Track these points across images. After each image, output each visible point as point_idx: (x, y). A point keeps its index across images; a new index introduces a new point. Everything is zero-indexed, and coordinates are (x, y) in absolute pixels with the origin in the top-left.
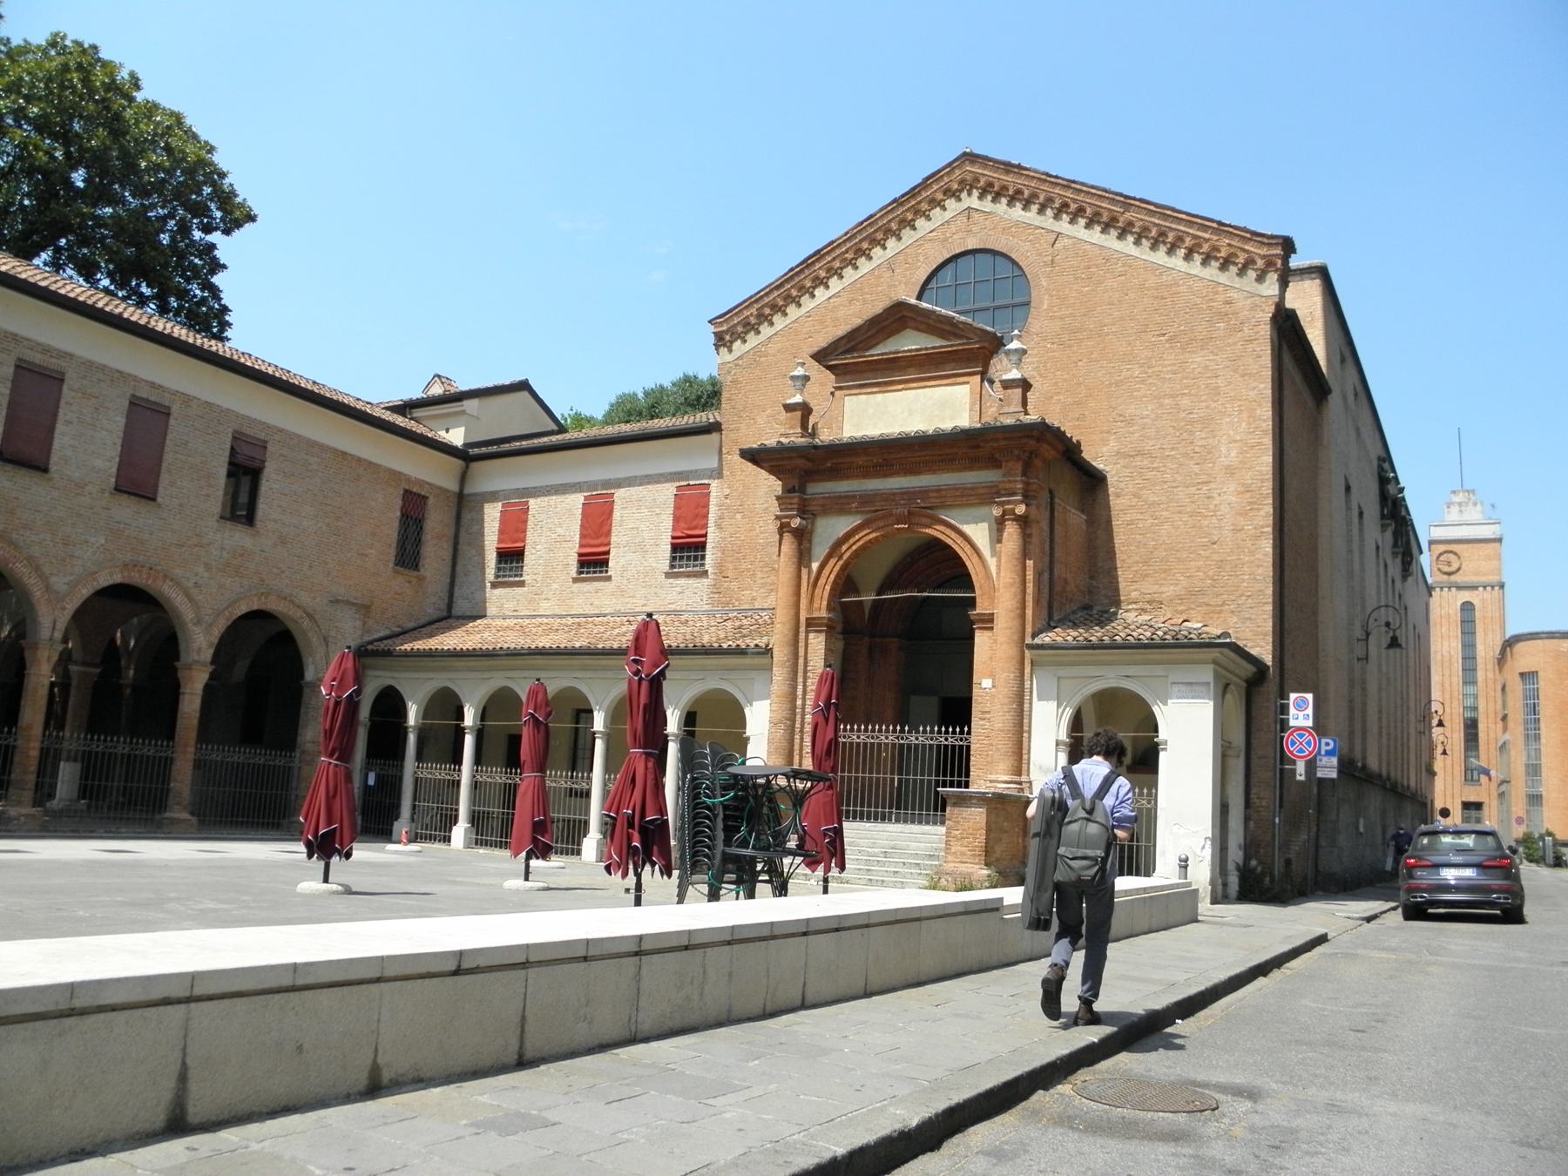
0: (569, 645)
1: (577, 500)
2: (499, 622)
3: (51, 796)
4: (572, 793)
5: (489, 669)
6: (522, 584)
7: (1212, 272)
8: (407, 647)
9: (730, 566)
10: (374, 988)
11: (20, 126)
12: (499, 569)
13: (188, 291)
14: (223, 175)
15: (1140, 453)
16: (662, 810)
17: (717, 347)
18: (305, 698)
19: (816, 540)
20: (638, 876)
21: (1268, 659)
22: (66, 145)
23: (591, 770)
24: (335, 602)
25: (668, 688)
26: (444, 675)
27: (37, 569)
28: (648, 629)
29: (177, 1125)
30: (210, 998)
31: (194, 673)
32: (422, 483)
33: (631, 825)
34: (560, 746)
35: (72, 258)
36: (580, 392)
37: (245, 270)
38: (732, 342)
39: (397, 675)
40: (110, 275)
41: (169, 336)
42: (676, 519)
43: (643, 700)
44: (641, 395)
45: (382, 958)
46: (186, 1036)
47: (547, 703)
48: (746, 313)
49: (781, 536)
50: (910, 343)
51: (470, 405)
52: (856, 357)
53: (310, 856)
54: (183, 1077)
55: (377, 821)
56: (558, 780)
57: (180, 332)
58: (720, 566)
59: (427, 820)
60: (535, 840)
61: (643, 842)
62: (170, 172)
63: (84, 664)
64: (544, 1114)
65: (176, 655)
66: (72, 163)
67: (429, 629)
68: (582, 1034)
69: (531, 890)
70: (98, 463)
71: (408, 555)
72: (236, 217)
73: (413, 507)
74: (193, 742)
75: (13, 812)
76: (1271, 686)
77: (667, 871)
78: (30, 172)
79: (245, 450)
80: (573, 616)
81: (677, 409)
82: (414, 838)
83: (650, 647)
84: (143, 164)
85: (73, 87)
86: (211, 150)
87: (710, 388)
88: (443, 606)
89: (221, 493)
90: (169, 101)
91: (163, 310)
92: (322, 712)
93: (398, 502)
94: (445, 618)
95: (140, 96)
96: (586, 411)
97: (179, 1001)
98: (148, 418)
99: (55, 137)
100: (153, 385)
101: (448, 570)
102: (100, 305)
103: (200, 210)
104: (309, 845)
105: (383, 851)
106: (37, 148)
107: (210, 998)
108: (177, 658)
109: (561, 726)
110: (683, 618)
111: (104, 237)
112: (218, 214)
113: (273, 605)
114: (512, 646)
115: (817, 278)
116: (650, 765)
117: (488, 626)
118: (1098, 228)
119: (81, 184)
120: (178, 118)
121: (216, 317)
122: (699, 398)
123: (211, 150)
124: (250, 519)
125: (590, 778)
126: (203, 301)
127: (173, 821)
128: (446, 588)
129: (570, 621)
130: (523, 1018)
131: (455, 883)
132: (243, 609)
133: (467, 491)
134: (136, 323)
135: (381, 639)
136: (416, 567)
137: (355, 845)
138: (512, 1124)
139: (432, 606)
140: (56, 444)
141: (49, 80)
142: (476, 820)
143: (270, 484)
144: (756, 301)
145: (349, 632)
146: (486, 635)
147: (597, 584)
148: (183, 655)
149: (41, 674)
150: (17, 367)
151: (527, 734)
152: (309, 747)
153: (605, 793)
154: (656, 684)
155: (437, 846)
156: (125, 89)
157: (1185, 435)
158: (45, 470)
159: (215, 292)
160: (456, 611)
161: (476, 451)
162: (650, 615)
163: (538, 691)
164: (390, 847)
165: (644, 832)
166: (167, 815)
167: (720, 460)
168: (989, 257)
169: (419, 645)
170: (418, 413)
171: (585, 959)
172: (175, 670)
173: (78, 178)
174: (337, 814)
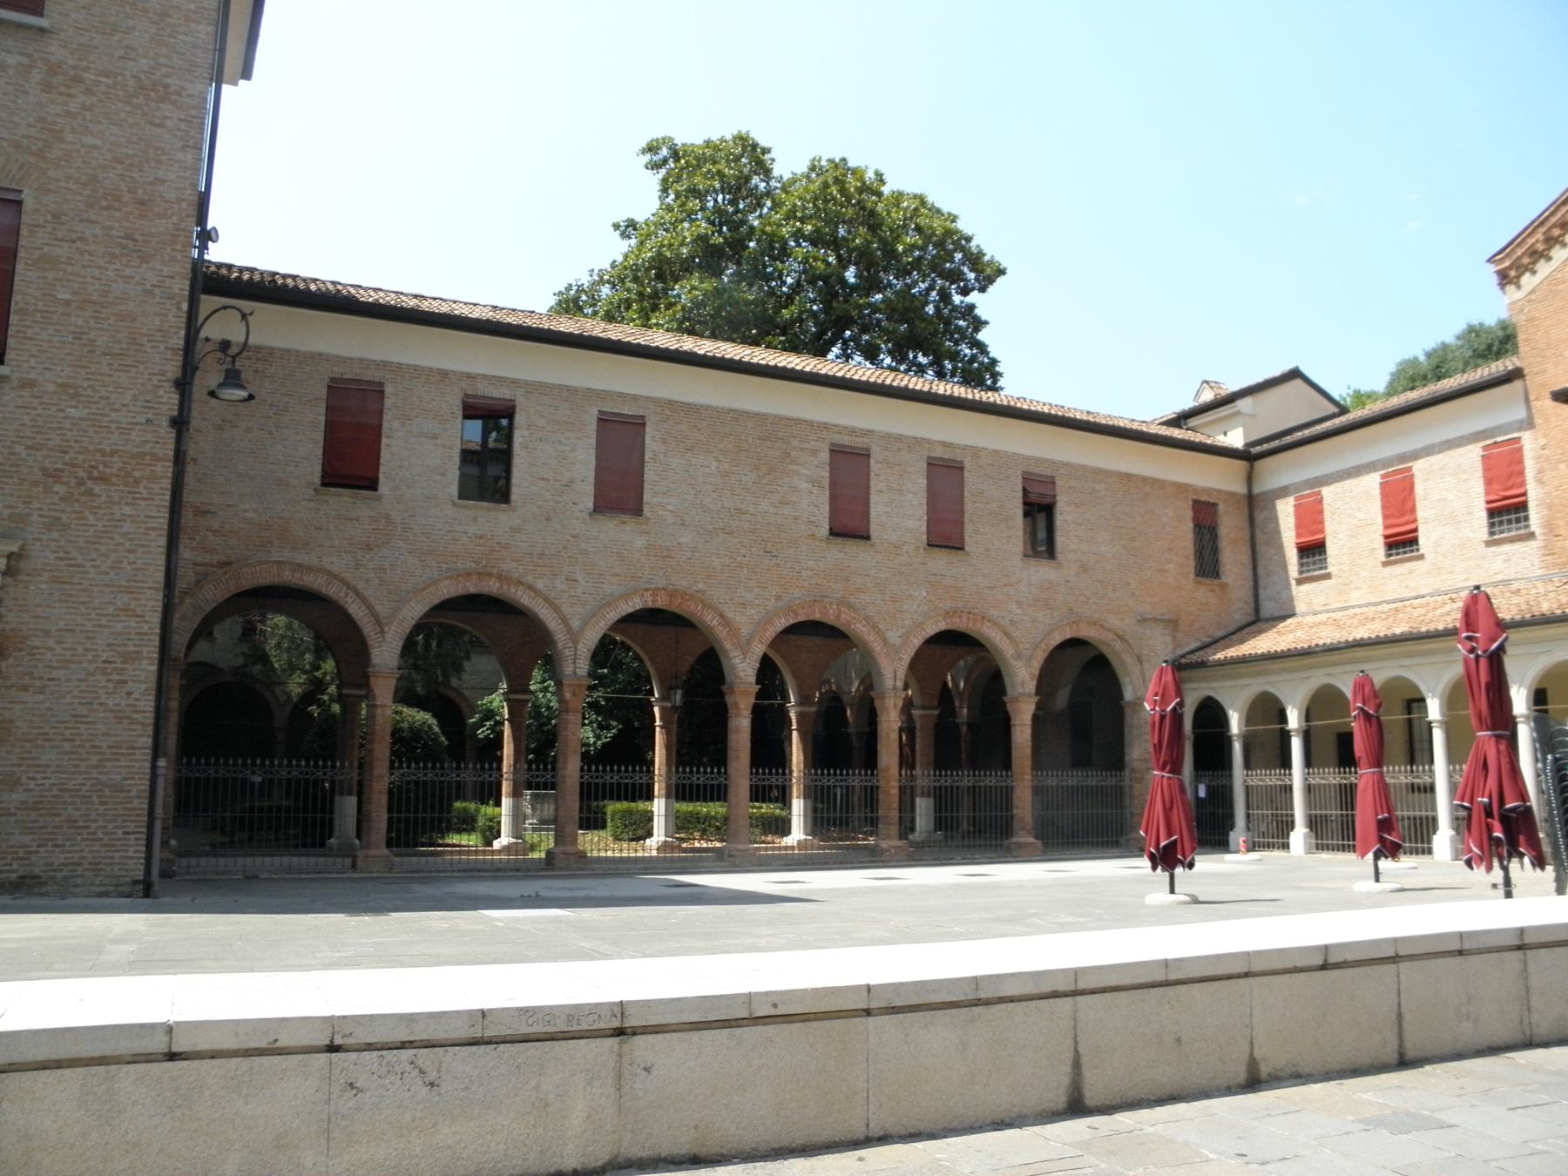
0: (1389, 633)
1: (1373, 481)
2: (1310, 619)
3: (912, 830)
4: (1413, 788)
5: (1309, 667)
6: (1328, 576)
8: (1220, 656)
9: (1561, 523)
10: (1242, 982)
11: (799, 245)
12: (1302, 565)
13: (958, 353)
14: (968, 239)
16: (1523, 796)
17: (1502, 285)
18: (1127, 719)
20: (1505, 869)
22: (836, 250)
23: (1432, 762)
24: (1143, 620)
25: (1511, 665)
26: (1261, 680)
27: (874, 627)
28: (1477, 606)
29: (1076, 1107)
30: (1093, 992)
31: (1022, 705)
32: (1209, 491)
33: (1489, 814)
34: (1395, 740)
35: (858, 347)
36: (1357, 369)
37: (1005, 321)
38: (1518, 277)
39: (1214, 685)
40: (890, 352)
41: (951, 397)
42: (1488, 482)
43: (1484, 678)
44: (1422, 358)
45: (1248, 954)
46: (1075, 1027)
47: (1376, 695)
48: (1531, 241)
51: (1244, 404)
53: (1154, 868)
54: (1077, 1064)
55: (1212, 829)
56: (1398, 775)
57: (960, 391)
58: (1550, 526)
59: (1263, 828)
60: (1382, 840)
61: (1506, 831)
62: (923, 248)
63: (924, 707)
64: (1437, 1115)
65: (1002, 690)
66: (843, 264)
67: (1239, 635)
68: (1466, 1034)
69: (1383, 892)
70: (911, 524)
71: (1207, 564)
72: (988, 273)
73: (1205, 516)
74: (1029, 770)
75: (884, 844)
77: (1539, 862)
78: (812, 282)
79: (1036, 489)
80: (1388, 602)
81: (1466, 364)
82: (1252, 847)
83: (1483, 623)
84: (901, 248)
85: (834, 199)
86: (954, 219)
87: (1500, 333)
88: (1250, 609)
89: (1021, 533)
90: (910, 188)
91: (941, 375)
92: (1148, 728)
93: (1189, 514)
94: (1253, 623)
95: (886, 190)
96: (1365, 388)
97: (1065, 995)
98: (945, 475)
99: (827, 245)
100: (944, 444)
101: (1249, 573)
102: (888, 382)
103: (955, 276)
104: (1152, 858)
105: (1223, 861)
106: (815, 259)
107: (1093, 992)
108: (1005, 693)
109: (1394, 718)
110: (1515, 586)
111: (879, 321)
112: (972, 276)
113: (1085, 632)
114: (1328, 641)
115: (1535, 252)
116: (1502, 747)
117: (1300, 625)
119: (852, 280)
120: (921, 199)
121: (987, 369)
122: (1490, 347)
123: (954, 219)
124: (1051, 553)
125: (1431, 771)
126: (973, 359)
127: (1020, 845)
128: (1250, 593)
129: (1386, 607)
130: (1400, 1017)
131: (1301, 888)
132: (1058, 639)
133: (1256, 490)
134: (921, 392)
135: (1193, 652)
136: (1217, 575)
137: (1197, 858)
138: (1403, 1123)
139: (1240, 614)
140: (873, 514)
141: (816, 199)
142: (1314, 823)
143: (1064, 516)
144: (1542, 224)
145: (1160, 648)
146: (1299, 633)
147: (1409, 565)
148: (1009, 689)
149: (890, 722)
150: (832, 451)
151: (1356, 727)
152: (1137, 764)
153: (1453, 787)
154: (1496, 660)
155: (1277, 853)
156: (871, 189)
158: (868, 538)
159: (982, 347)
160: (1264, 613)
161: (1258, 449)
162: (1477, 587)
163: (1363, 685)
164: (1228, 857)
165: (1506, 820)
166: (1015, 840)
167: (1529, 408)
169: (1232, 652)
170: (1193, 422)
171: (1460, 953)
172: (1004, 704)
173: (850, 275)
174: (1175, 822)
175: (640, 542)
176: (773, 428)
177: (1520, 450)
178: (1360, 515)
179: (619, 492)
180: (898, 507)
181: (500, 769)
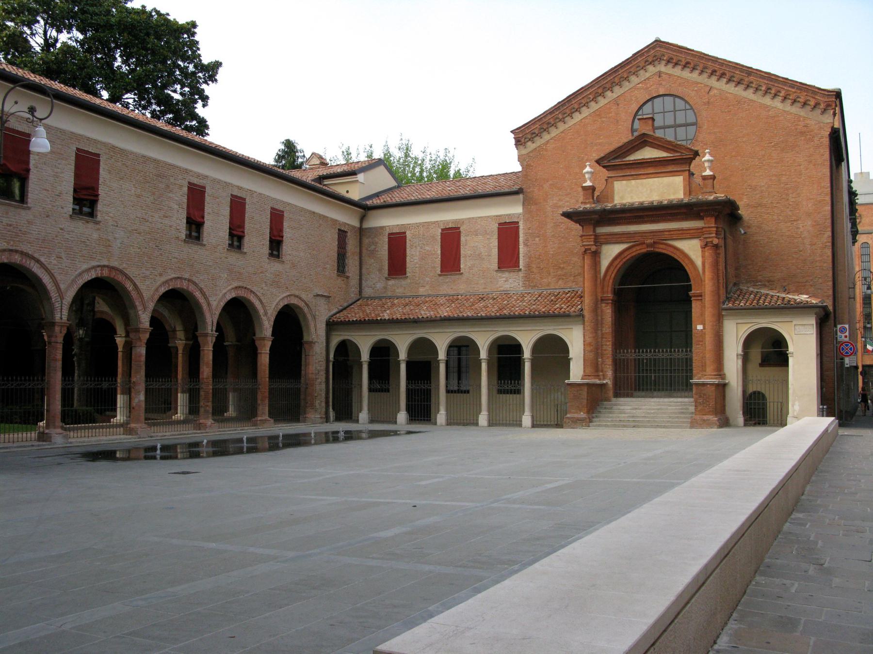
7: (795, 110)
9: (534, 266)
15: (760, 205)
19: (602, 256)
21: (831, 308)
49: (584, 258)
50: (648, 153)
52: (617, 162)
58: (528, 266)
70: (221, 234)
73: (342, 235)
76: (831, 321)
118: (733, 84)
157: (784, 196)
160: (368, 292)
168: (671, 98)
170: (326, 182)
175: (95, 236)
176: (162, 171)
177: (518, 228)
178: (427, 248)
179: (86, 200)
180: (216, 224)
181: (116, 381)
